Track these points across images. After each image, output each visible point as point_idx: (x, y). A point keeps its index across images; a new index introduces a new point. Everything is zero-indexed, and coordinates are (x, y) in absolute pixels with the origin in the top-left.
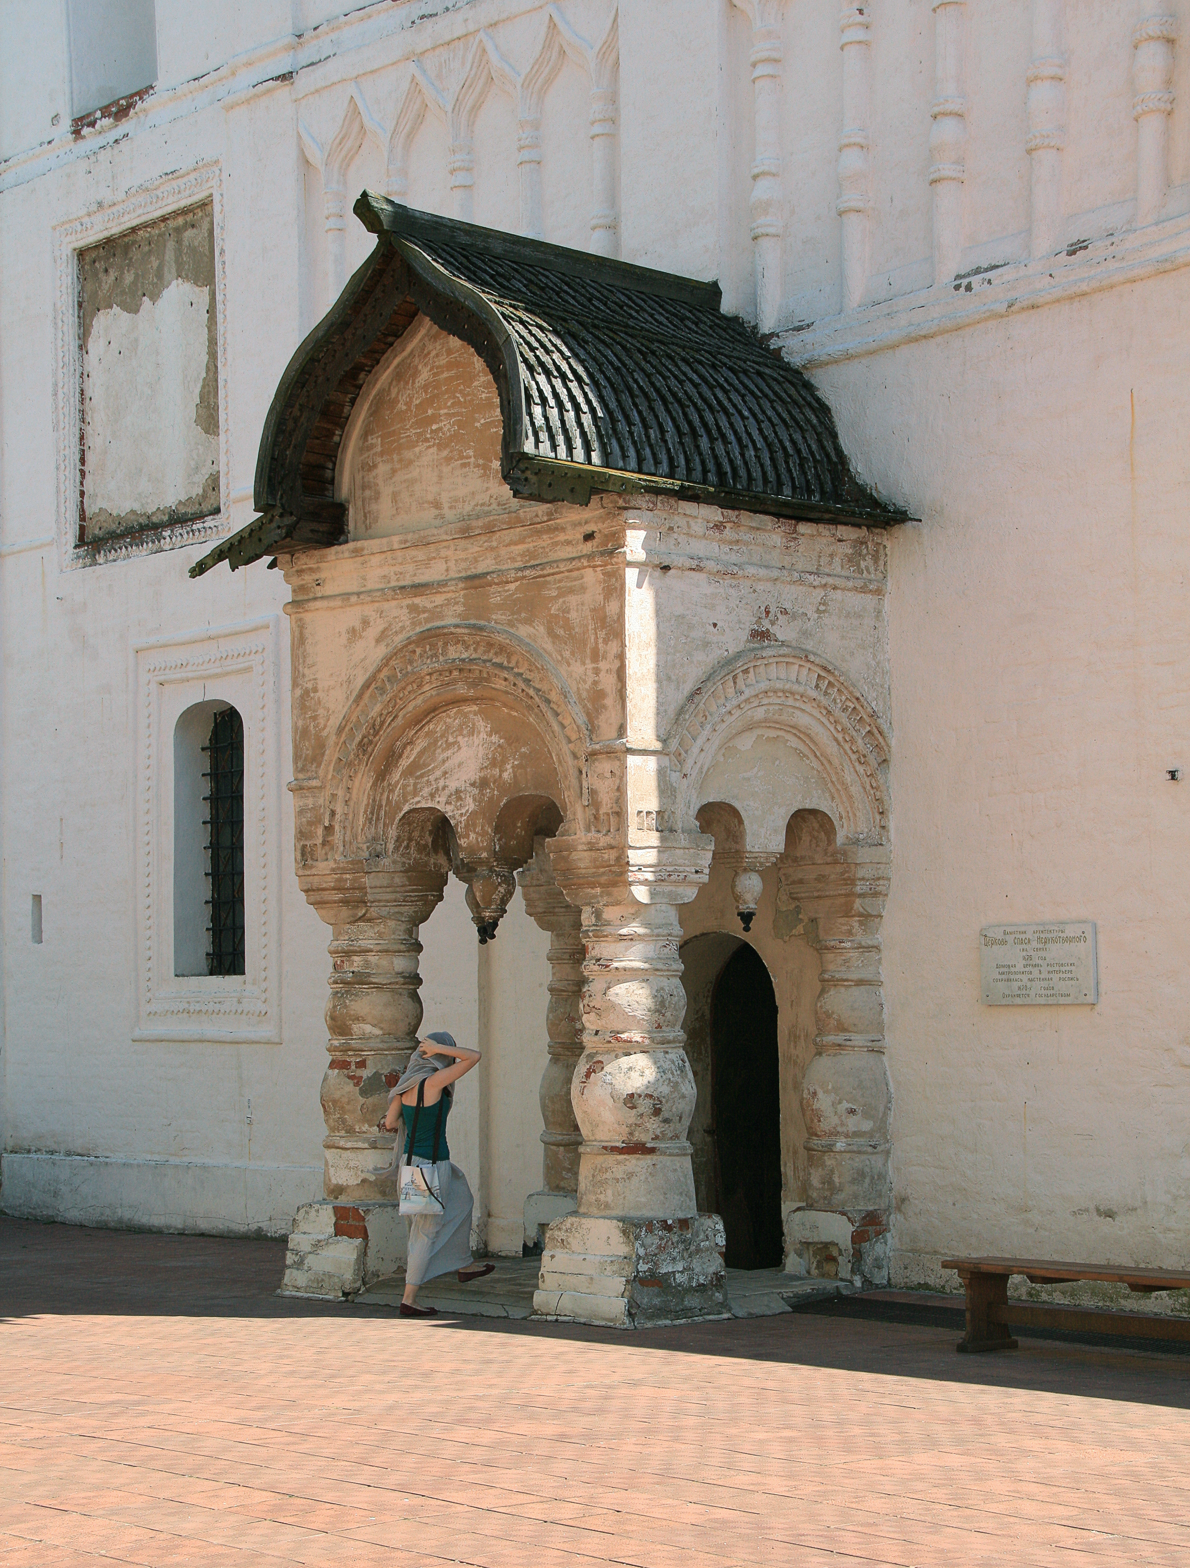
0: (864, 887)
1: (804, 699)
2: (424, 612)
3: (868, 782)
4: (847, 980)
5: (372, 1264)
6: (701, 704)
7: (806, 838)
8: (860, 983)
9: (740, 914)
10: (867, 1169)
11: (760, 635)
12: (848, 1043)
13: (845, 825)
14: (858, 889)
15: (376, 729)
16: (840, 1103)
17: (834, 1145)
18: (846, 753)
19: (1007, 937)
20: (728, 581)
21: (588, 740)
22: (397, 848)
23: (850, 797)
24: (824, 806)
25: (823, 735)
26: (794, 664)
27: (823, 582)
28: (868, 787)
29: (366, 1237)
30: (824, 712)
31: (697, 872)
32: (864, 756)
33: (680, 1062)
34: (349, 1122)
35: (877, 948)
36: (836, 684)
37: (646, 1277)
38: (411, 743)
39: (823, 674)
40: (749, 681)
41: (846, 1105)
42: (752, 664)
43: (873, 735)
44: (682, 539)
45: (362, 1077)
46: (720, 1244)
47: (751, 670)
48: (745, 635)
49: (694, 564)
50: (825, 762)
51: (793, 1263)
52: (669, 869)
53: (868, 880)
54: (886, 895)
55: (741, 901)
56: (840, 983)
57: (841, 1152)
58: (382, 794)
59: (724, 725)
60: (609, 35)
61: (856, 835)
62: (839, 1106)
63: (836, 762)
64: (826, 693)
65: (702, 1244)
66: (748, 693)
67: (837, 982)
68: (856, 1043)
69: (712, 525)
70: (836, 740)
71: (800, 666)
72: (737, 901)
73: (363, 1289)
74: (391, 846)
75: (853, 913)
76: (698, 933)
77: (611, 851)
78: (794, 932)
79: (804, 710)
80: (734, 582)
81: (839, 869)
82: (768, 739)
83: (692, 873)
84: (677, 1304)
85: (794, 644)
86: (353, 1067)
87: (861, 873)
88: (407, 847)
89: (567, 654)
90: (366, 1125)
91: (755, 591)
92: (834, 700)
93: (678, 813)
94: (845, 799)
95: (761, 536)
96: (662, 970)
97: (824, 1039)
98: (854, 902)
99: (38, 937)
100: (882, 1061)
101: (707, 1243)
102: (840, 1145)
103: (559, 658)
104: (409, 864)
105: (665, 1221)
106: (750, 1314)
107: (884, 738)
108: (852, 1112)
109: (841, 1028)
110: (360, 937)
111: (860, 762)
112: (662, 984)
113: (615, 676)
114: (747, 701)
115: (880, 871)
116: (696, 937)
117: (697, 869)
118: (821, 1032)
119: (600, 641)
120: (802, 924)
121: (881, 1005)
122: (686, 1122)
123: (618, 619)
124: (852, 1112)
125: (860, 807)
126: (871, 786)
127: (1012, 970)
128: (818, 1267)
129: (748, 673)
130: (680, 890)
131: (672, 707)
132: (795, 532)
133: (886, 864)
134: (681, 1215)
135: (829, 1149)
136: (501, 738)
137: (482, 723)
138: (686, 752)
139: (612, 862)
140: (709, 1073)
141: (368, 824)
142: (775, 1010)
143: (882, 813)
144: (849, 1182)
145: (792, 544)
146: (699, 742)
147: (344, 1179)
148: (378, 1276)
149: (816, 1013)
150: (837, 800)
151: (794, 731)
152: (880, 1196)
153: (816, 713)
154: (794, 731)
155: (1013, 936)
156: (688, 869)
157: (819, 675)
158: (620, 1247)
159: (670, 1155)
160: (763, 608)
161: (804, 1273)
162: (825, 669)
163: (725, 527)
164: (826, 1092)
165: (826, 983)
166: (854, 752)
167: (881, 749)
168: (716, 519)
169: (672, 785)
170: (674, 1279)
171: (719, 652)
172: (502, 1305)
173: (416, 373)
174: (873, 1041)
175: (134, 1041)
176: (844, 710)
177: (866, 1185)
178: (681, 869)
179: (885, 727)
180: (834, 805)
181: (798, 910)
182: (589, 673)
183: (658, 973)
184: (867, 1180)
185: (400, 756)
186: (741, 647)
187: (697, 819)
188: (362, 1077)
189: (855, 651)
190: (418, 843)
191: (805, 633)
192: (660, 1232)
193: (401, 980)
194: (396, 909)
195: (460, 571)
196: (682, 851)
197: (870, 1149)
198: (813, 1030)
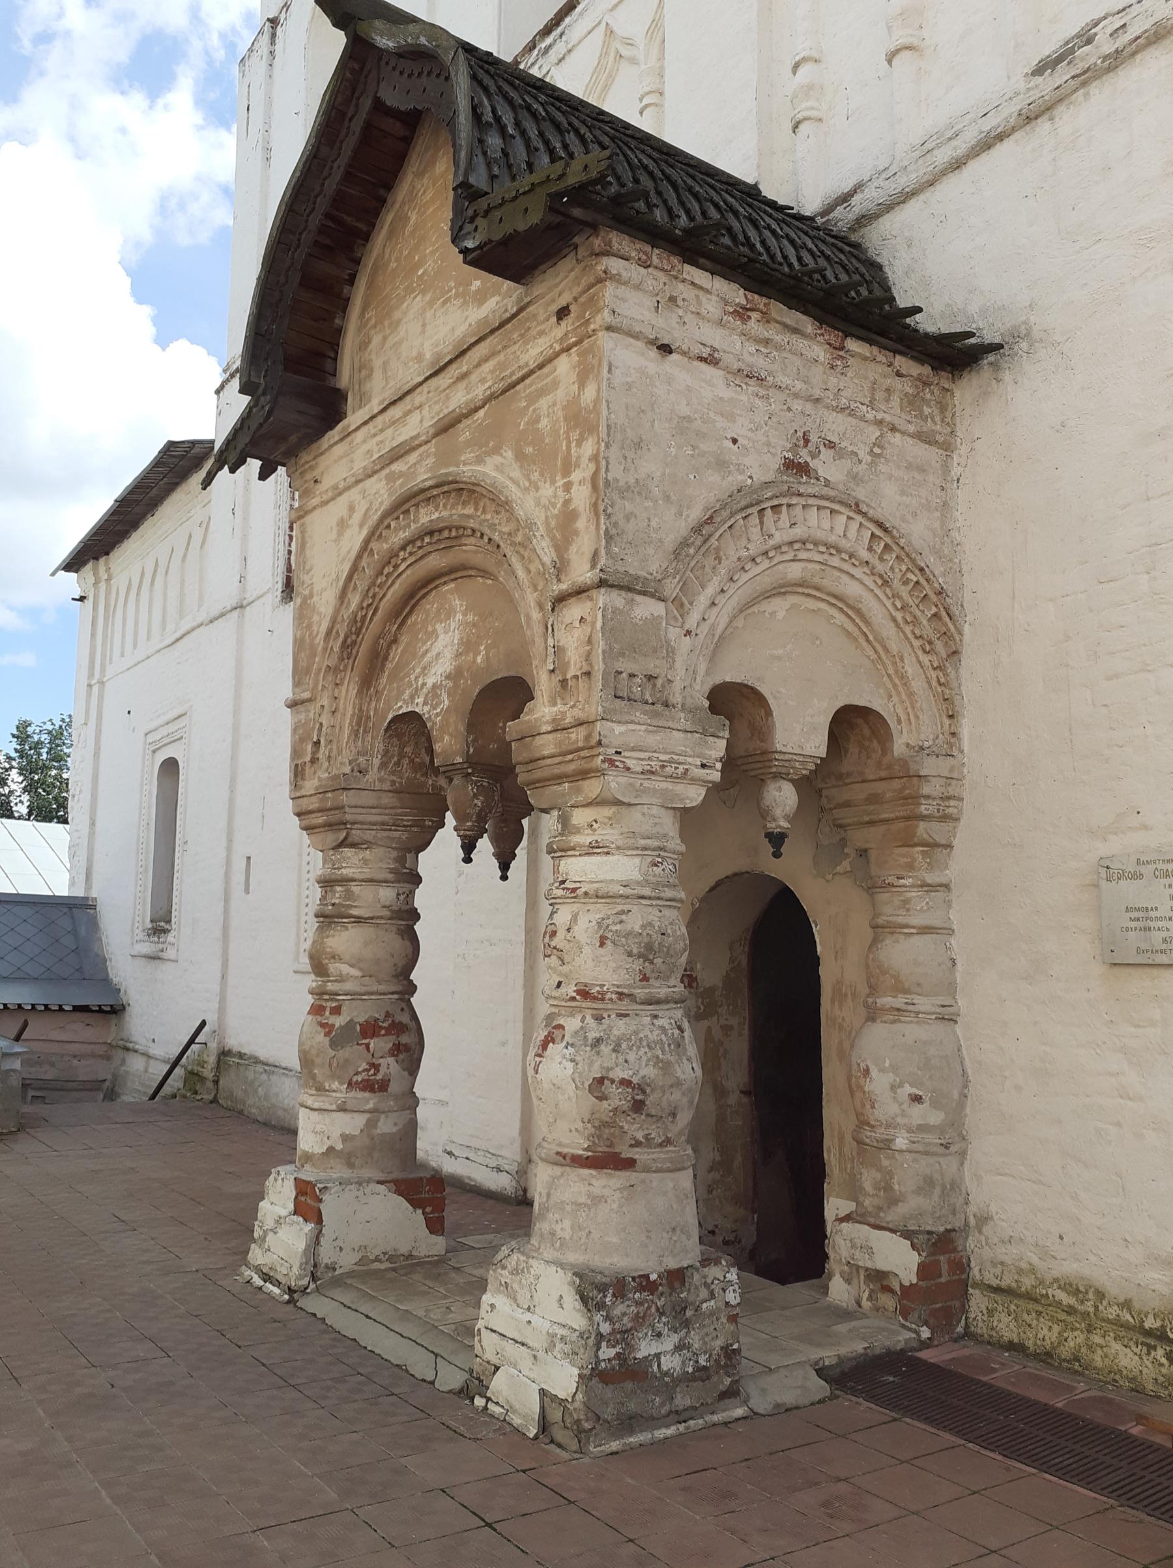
0: (931, 808)
1: (853, 560)
2: (399, 478)
3: (934, 676)
4: (907, 926)
5: (326, 1255)
6: (713, 540)
7: (853, 749)
8: (925, 930)
9: (769, 836)
10: (936, 1176)
11: (796, 467)
12: (911, 1008)
13: (904, 731)
14: (923, 809)
15: (357, 625)
16: (901, 1086)
17: (891, 1141)
18: (907, 638)
19: (1142, 869)
20: (753, 387)
21: (555, 581)
22: (383, 765)
23: (911, 695)
24: (877, 705)
25: (877, 611)
26: (841, 513)
27: (879, 417)
28: (934, 683)
29: (319, 1221)
30: (880, 582)
31: (703, 766)
32: (930, 643)
33: (677, 1032)
34: (320, 1078)
35: (947, 886)
36: (894, 547)
37: (613, 1369)
38: (395, 641)
39: (878, 532)
40: (781, 524)
41: (909, 1089)
42: (784, 501)
43: (940, 619)
44: (689, 318)
45: (333, 1025)
46: (733, 1302)
47: (784, 508)
48: (776, 463)
49: (705, 352)
50: (879, 649)
51: (839, 1290)
52: (663, 757)
53: (934, 799)
54: (958, 819)
55: (768, 819)
56: (898, 930)
57: (901, 1151)
58: (369, 704)
59: (745, 577)
60: (656, 12)
61: (921, 743)
62: (898, 1091)
63: (894, 648)
64: (881, 559)
65: (705, 1305)
66: (778, 538)
67: (894, 928)
68: (922, 1009)
69: (731, 310)
70: (894, 620)
71: (849, 518)
72: (764, 818)
73: (312, 1286)
74: (376, 762)
75: (916, 840)
76: (729, 873)
77: (580, 729)
78: (839, 869)
79: (853, 576)
80: (762, 392)
81: (896, 784)
82: (808, 610)
83: (696, 766)
84: (662, 1404)
85: (841, 487)
86: (327, 1013)
87: (926, 790)
88: (398, 763)
89: (535, 476)
90: (336, 1083)
91: (789, 409)
92: (892, 568)
93: (678, 685)
94: (904, 697)
95: (801, 343)
96: (650, 898)
97: (878, 1000)
98: (917, 826)
99: (247, 891)
100: (955, 1033)
101: (712, 1303)
102: (901, 1142)
103: (527, 484)
104: (401, 783)
105: (647, 1277)
106: (777, 1406)
107: (954, 624)
108: (917, 1099)
109: (900, 988)
110: (344, 865)
111: (924, 651)
112: (651, 918)
113: (590, 486)
114: (777, 548)
115: (950, 789)
116: (727, 877)
117: (705, 761)
118: (873, 990)
119: (573, 445)
120: (848, 860)
121: (953, 960)
122: (684, 1118)
123: (595, 406)
124: (917, 1099)
125: (924, 706)
126: (939, 681)
127: (1152, 914)
128: (870, 1298)
129: (780, 513)
130: (679, 788)
131: (672, 536)
132: (842, 348)
133: (958, 779)
134: (673, 1264)
135: (886, 1145)
136: (474, 615)
137: (457, 602)
138: (691, 604)
139: (580, 744)
140: (746, 1027)
141: (353, 737)
142: (816, 961)
143: (951, 717)
144: (913, 1192)
145: (839, 363)
146: (711, 590)
147: (310, 1145)
148: (335, 1269)
149: (867, 967)
150: (895, 698)
151: (840, 605)
152: (954, 1212)
153: (868, 581)
154: (840, 605)
155: (1152, 867)
156: (689, 760)
157: (872, 534)
158: (574, 1317)
159: (658, 1171)
160: (800, 434)
161: (852, 1305)
162: (880, 525)
163: (749, 317)
164: (882, 1070)
165: (880, 930)
166: (917, 638)
167: (951, 638)
168: (737, 300)
169: (669, 644)
170: (659, 1366)
171: (740, 477)
172: (436, 1355)
173: (407, 218)
174: (943, 1006)
175: (296, 972)
176: (906, 582)
177: (936, 1197)
178: (681, 759)
179: (955, 611)
180: (891, 705)
181: (843, 842)
182: (560, 493)
183: (644, 902)
184: (937, 1191)
185: (386, 658)
186: (770, 477)
187: (708, 698)
188: (333, 1025)
189: (918, 512)
190: (412, 761)
191: (855, 477)
192: (637, 1295)
193: (386, 913)
194: (386, 834)
195: (433, 417)
196: (681, 735)
197: (941, 1150)
198: (864, 989)
